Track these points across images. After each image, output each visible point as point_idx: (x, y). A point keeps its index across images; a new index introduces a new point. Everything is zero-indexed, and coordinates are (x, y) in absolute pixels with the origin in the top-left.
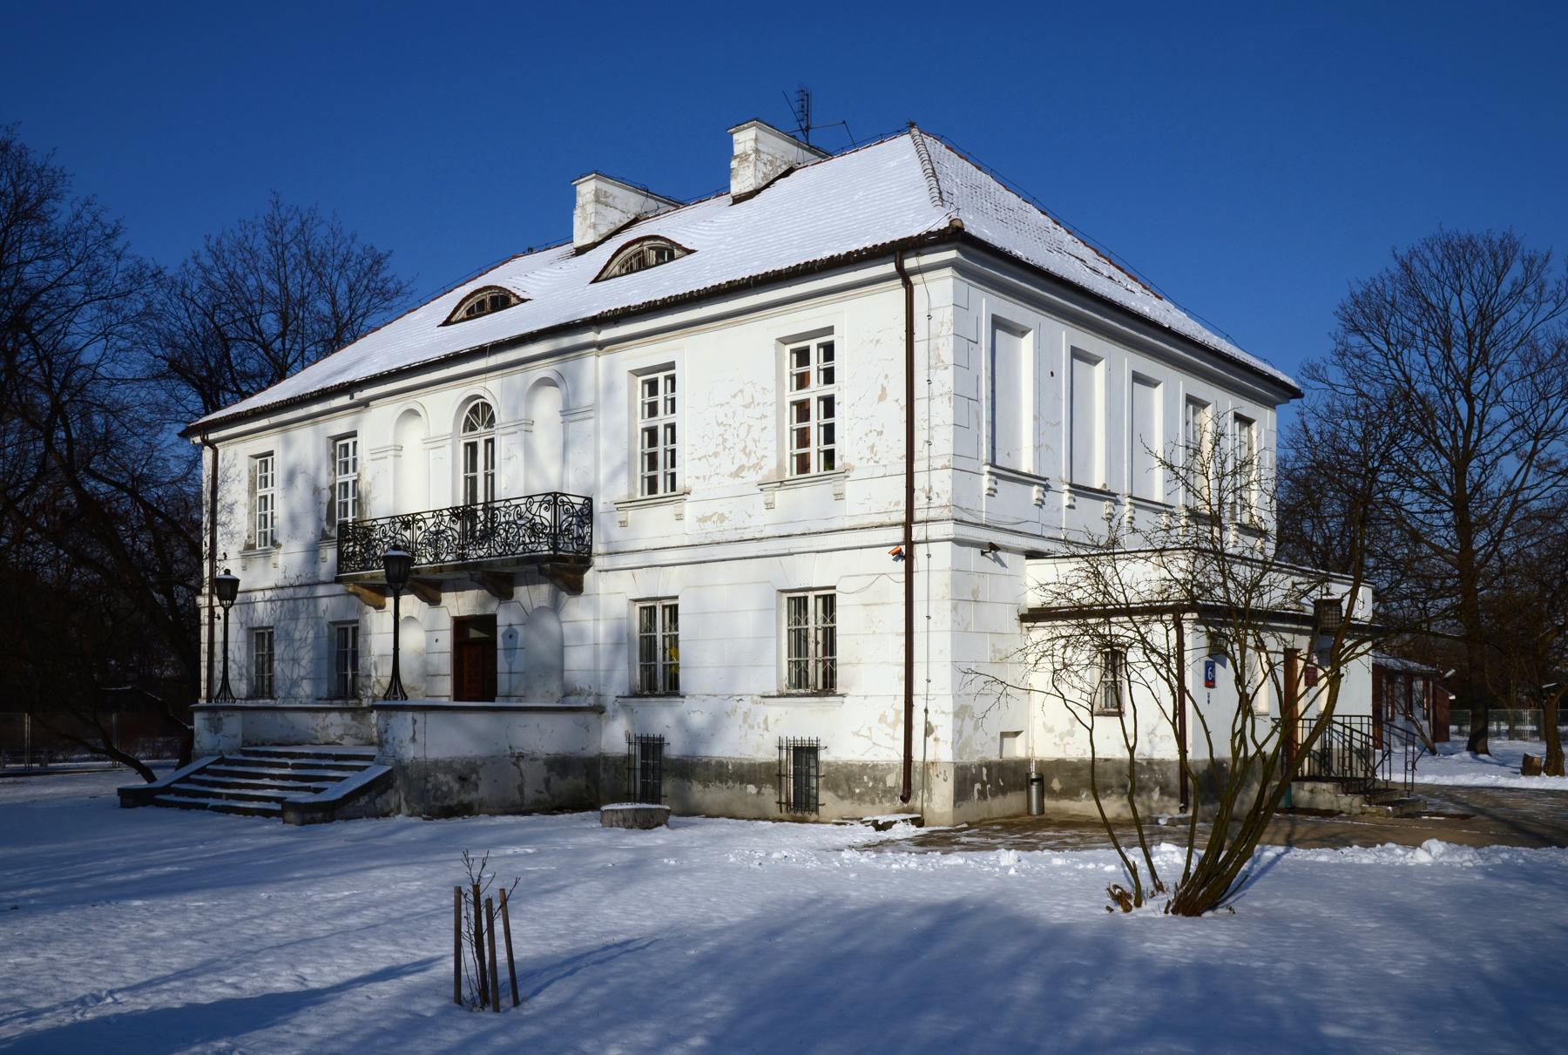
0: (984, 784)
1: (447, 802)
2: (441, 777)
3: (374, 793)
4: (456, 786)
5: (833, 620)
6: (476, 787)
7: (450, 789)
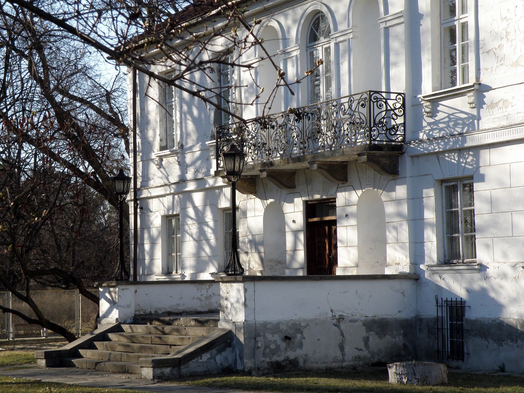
1: (275, 358)
3: (214, 351)
4: (283, 345)
5: (472, 204)
6: (301, 346)
7: (278, 347)
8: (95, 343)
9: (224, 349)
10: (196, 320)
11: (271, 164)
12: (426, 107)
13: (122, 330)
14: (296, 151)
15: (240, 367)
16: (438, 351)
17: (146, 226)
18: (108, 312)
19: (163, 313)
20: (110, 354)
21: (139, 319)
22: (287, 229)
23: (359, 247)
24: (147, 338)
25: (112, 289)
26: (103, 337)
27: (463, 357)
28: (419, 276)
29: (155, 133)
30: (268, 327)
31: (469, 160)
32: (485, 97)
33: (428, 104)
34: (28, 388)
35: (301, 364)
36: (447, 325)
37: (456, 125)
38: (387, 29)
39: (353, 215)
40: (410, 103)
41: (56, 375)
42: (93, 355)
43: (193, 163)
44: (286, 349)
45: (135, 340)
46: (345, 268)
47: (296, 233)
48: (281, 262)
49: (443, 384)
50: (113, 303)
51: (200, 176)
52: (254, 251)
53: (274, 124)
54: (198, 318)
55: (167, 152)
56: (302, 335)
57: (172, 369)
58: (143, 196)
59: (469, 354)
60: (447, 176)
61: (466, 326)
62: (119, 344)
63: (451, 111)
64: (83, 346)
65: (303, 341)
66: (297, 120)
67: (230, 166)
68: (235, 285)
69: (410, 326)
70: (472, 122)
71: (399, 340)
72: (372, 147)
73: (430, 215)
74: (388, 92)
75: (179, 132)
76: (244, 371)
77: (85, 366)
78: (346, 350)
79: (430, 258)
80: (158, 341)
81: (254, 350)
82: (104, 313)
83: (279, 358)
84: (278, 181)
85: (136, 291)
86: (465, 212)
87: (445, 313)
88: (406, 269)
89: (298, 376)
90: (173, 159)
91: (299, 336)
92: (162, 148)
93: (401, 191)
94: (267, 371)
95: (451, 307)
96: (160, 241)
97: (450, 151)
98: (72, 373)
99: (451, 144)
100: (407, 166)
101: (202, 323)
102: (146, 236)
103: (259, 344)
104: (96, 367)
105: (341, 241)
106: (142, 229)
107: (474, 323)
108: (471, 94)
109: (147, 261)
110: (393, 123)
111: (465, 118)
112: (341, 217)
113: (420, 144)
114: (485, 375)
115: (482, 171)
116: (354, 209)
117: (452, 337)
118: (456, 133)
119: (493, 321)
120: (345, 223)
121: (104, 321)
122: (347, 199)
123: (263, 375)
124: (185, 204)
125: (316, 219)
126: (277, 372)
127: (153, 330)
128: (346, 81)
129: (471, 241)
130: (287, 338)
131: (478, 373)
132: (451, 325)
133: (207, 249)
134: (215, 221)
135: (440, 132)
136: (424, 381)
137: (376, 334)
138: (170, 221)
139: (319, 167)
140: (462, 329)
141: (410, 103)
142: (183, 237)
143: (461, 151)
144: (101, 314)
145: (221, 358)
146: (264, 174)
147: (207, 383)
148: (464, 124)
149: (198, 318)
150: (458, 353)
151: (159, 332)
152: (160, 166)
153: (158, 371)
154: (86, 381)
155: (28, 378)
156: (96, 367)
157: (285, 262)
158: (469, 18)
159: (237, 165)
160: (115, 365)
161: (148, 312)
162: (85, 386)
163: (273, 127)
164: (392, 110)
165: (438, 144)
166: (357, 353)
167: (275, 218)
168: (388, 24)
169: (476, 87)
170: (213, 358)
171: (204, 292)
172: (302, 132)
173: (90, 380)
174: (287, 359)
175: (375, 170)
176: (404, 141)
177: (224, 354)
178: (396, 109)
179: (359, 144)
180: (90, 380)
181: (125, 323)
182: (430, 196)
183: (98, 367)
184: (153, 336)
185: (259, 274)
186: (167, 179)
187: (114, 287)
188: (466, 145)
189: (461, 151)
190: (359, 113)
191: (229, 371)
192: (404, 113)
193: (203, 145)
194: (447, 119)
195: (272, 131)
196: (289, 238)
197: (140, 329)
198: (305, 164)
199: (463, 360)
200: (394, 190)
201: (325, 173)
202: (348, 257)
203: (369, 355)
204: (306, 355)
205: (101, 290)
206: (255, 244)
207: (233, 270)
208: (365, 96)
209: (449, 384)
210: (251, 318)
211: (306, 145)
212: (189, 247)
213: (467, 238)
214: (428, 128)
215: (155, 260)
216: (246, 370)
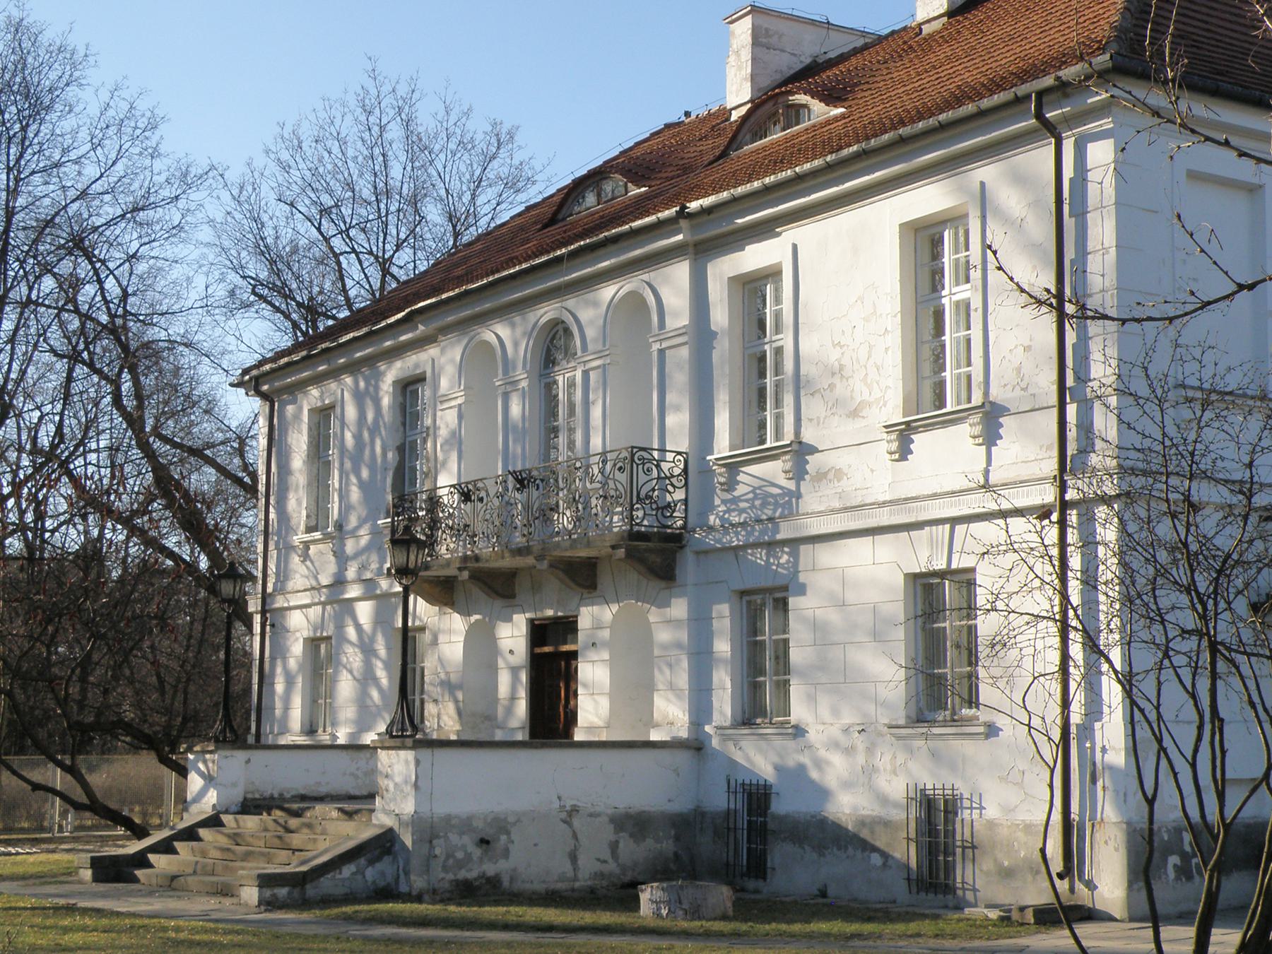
0: (1185, 857)
1: (463, 874)
2: (454, 838)
3: (362, 861)
4: (477, 852)
5: (785, 630)
6: (506, 854)
7: (468, 857)
8: (176, 844)
9: (379, 859)
10: (340, 810)
11: (477, 558)
12: (720, 475)
13: (221, 824)
14: (518, 540)
15: (403, 888)
16: (727, 864)
17: (280, 652)
18: (202, 793)
19: (293, 797)
20: (197, 863)
22: (501, 663)
23: (612, 696)
24: (259, 838)
25: (208, 756)
26: (190, 834)
27: (765, 873)
28: (702, 743)
29: (298, 505)
30: (453, 822)
31: (783, 561)
32: (807, 462)
33: (723, 470)
34: (48, 917)
35: (506, 884)
36: (743, 822)
37: (764, 505)
39: (605, 644)
40: (696, 470)
41: (104, 896)
42: (169, 864)
43: (356, 556)
44: (481, 859)
45: (239, 841)
46: (590, 729)
47: (514, 671)
48: (489, 718)
49: (724, 918)
50: (209, 779)
51: (368, 575)
52: (447, 698)
53: (483, 494)
54: (346, 806)
55: (317, 535)
56: (509, 838)
57: (294, 890)
58: (277, 605)
59: (774, 869)
60: (749, 584)
61: (771, 826)
62: (215, 847)
63: (757, 483)
64: (154, 849)
65: (511, 846)
66: (518, 490)
67: (401, 559)
68: (403, 754)
69: (685, 825)
70: (789, 502)
71: (668, 846)
73: (722, 646)
74: (663, 450)
75: (336, 506)
76: (410, 894)
77: (154, 881)
78: (580, 862)
79: (721, 713)
80: (277, 842)
81: (428, 860)
84: (489, 586)
85: (248, 761)
86: (776, 642)
87: (739, 804)
88: (684, 734)
89: (497, 903)
90: (326, 548)
91: (504, 838)
92: (309, 530)
93: (679, 608)
94: (448, 895)
95: (750, 795)
96: (300, 680)
97: (755, 545)
98: (131, 894)
99: (757, 534)
100: (688, 566)
101: (349, 815)
102: (279, 670)
103: (437, 851)
104: (172, 883)
105: (585, 686)
106: (273, 659)
107: (782, 819)
108: (788, 457)
109: (278, 712)
110: (669, 498)
111: (779, 495)
112: (586, 648)
113: (709, 533)
114: (795, 902)
115: (802, 578)
116: (606, 634)
117: (749, 841)
118: (764, 517)
119: (812, 817)
120: (593, 655)
121: (194, 809)
122: (594, 617)
123: (442, 901)
124: (343, 621)
125: (547, 649)
126: (465, 897)
127: (271, 825)
128: (598, 432)
129: (783, 688)
130: (484, 842)
131: (784, 899)
132: (749, 822)
133: (375, 694)
134: (388, 649)
135: (740, 515)
136: (695, 913)
137: (631, 835)
138: (318, 647)
139: (551, 566)
140: (766, 830)
141: (696, 470)
142: (336, 672)
143: (772, 545)
144: (189, 798)
145: (373, 874)
146: (466, 574)
147: (344, 913)
148: (776, 505)
149: (346, 806)
150: (758, 867)
151: (280, 829)
152: (305, 556)
153: (268, 893)
154: (150, 908)
155: (56, 900)
156: (172, 883)
157: (496, 718)
158: (786, 341)
159: (412, 557)
160: (203, 882)
161: (267, 794)
162: (142, 916)
163: (481, 500)
164: (666, 477)
165: (737, 534)
166: (598, 867)
167: (482, 645)
168: (664, 345)
169: (795, 447)
170: (359, 872)
172: (527, 507)
173: (157, 905)
174: (482, 875)
175: (640, 573)
176: (684, 527)
177: (379, 866)
178: (673, 476)
179: (615, 530)
180: (157, 905)
181: (227, 812)
182: (723, 616)
183: (175, 884)
184: (268, 834)
185: (453, 737)
186: (316, 579)
187: (211, 752)
188: (779, 537)
189: (772, 545)
190: (615, 480)
191: (386, 893)
192: (686, 484)
193: (375, 525)
194: (751, 496)
195: (480, 505)
196: (504, 680)
197: (251, 823)
198: (530, 560)
199: (765, 879)
200: (669, 605)
201: (561, 574)
202: (593, 711)
203: (618, 871)
204: (515, 870)
205: (191, 756)
206: (449, 687)
207: (407, 728)
208: (625, 454)
209: (735, 918)
210: (425, 809)
211: (532, 530)
212: (346, 688)
213: (778, 684)
214: (722, 508)
215: (290, 710)
216: (414, 893)
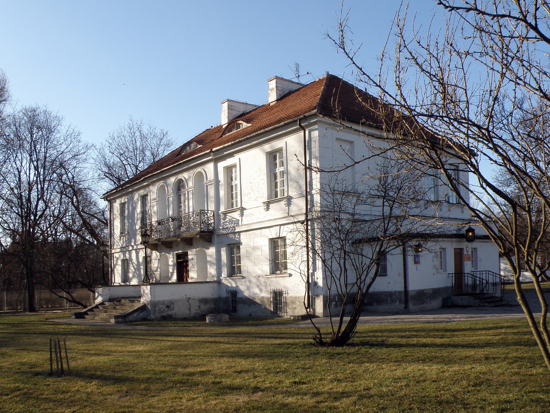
1: (163, 314)
2: (161, 306)
3: (139, 312)
4: (166, 309)
5: (239, 253)
6: (173, 309)
7: (164, 310)
15: (149, 318)
21: (111, 300)
35: (174, 316)
36: (230, 299)
38: (207, 186)
60: (230, 243)
61: (237, 300)
67: (144, 240)
69: (217, 301)
71: (212, 306)
72: (201, 232)
74: (208, 210)
82: (376, 290)
83: (165, 314)
87: (230, 296)
100: (215, 239)
107: (240, 298)
130: (168, 307)
139: (181, 240)
148: (235, 223)
150: (234, 310)
153: (117, 320)
166: (196, 311)
171: (137, 289)
176: (214, 229)
177: (143, 313)
210: (153, 299)
